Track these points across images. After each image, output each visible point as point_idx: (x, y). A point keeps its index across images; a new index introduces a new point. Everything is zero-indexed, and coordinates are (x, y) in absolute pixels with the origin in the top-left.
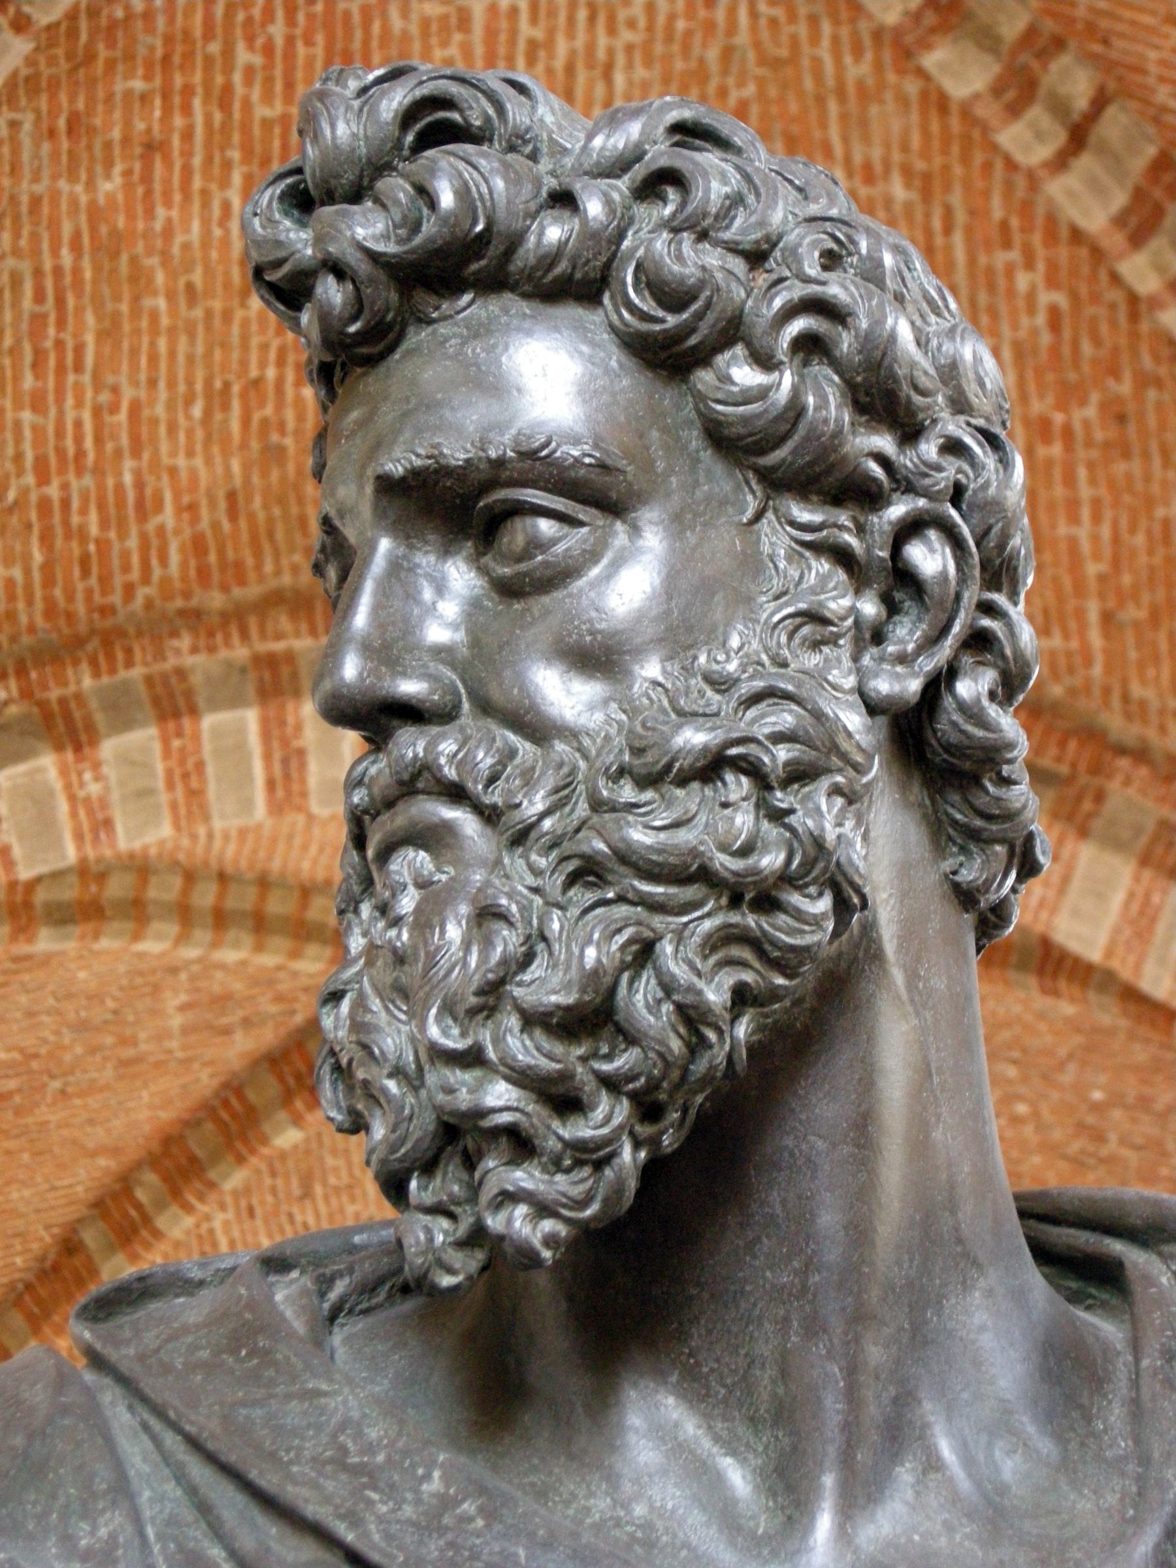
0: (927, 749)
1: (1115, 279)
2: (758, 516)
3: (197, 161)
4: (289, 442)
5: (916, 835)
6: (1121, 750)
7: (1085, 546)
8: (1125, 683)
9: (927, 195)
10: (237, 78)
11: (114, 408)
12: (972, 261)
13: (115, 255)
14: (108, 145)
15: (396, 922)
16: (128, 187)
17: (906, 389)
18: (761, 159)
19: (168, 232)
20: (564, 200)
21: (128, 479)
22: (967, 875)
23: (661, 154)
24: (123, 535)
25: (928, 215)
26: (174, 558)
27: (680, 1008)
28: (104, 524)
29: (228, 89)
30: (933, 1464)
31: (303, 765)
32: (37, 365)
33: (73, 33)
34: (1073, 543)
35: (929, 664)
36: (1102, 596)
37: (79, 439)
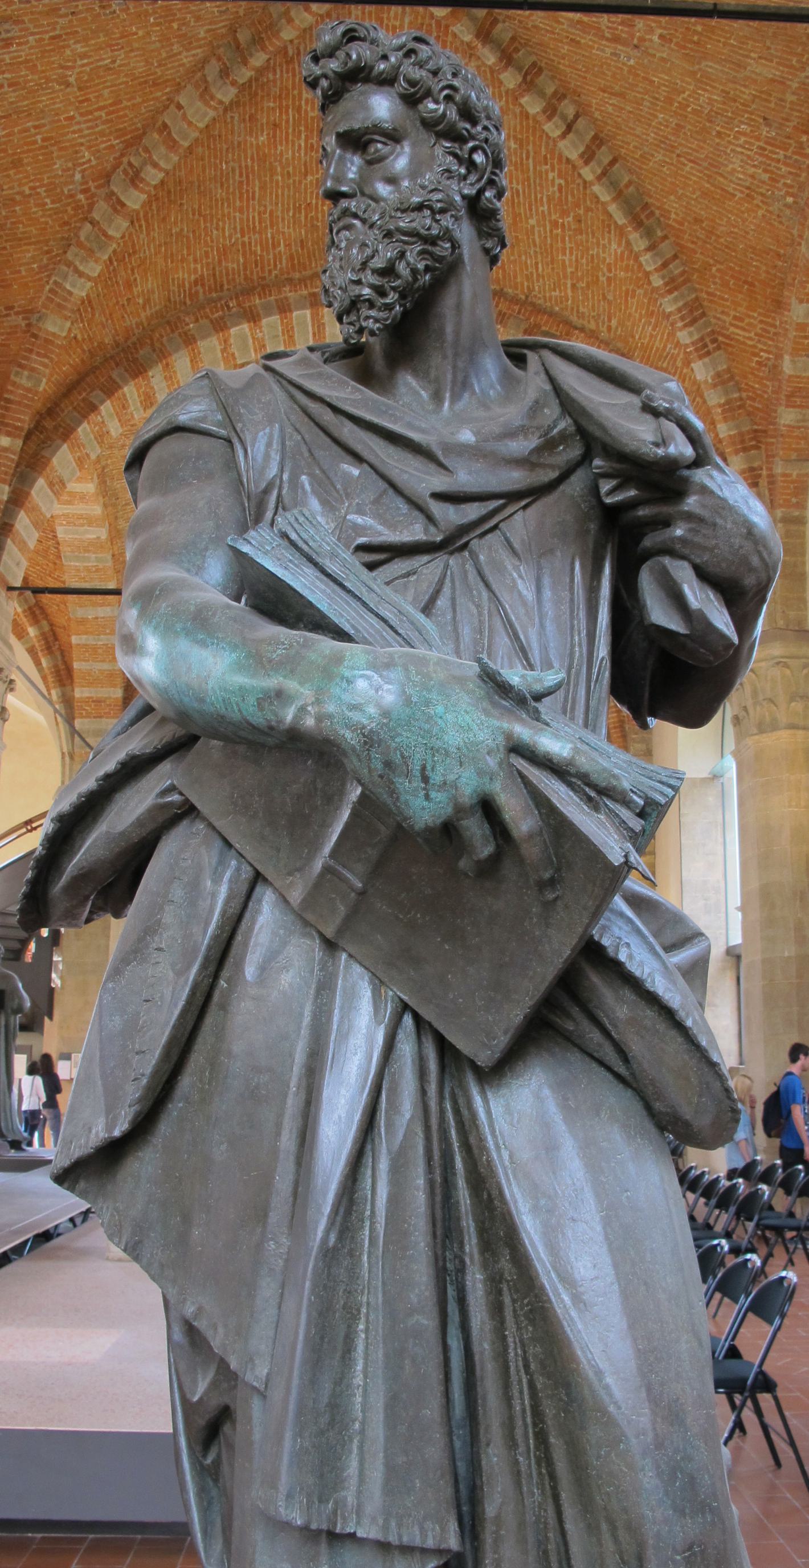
0: (480, 213)
1: (580, 175)
2: (434, 144)
3: (290, 131)
4: (319, 224)
5: (474, 233)
6: (576, 328)
7: (567, 263)
8: (578, 307)
9: (521, 146)
10: (303, 103)
11: (265, 213)
12: (535, 168)
13: (265, 161)
14: (262, 124)
15: (340, 249)
16: (269, 139)
17: (473, 111)
18: (438, 48)
19: (281, 154)
20: (385, 57)
21: (269, 235)
22: (489, 245)
23: (412, 45)
24: (268, 254)
25: (522, 154)
26: (284, 261)
27: (412, 269)
28: (262, 250)
29: (300, 106)
30: (474, 393)
31: (324, 328)
32: (241, 198)
33: (250, 87)
34: (564, 261)
35: (478, 186)
36: (572, 279)
37: (254, 223)
